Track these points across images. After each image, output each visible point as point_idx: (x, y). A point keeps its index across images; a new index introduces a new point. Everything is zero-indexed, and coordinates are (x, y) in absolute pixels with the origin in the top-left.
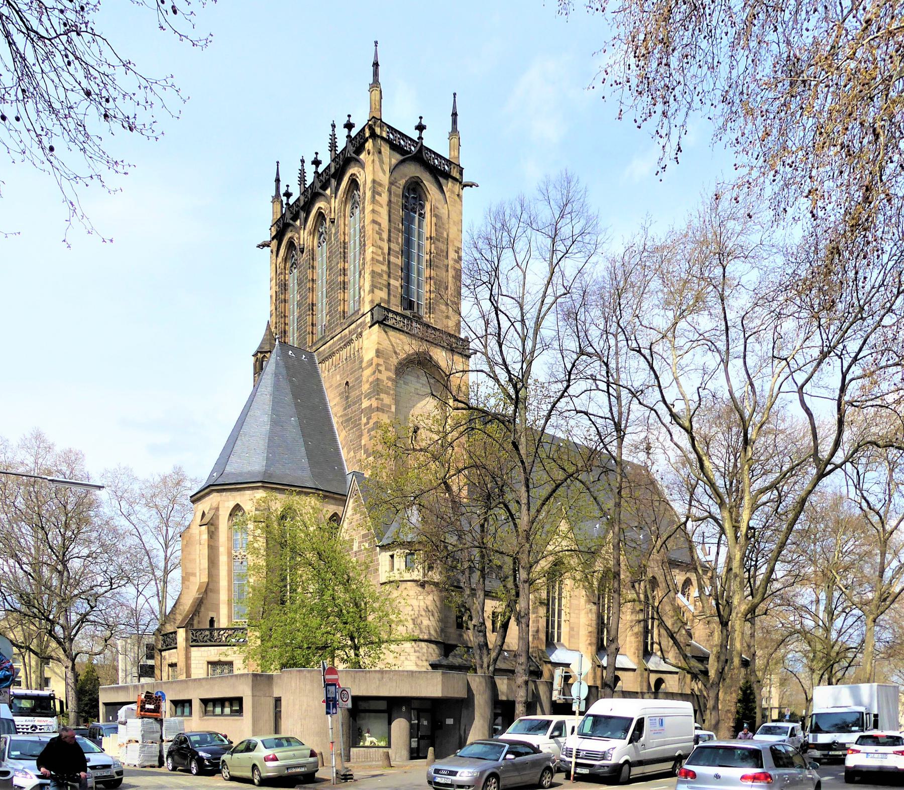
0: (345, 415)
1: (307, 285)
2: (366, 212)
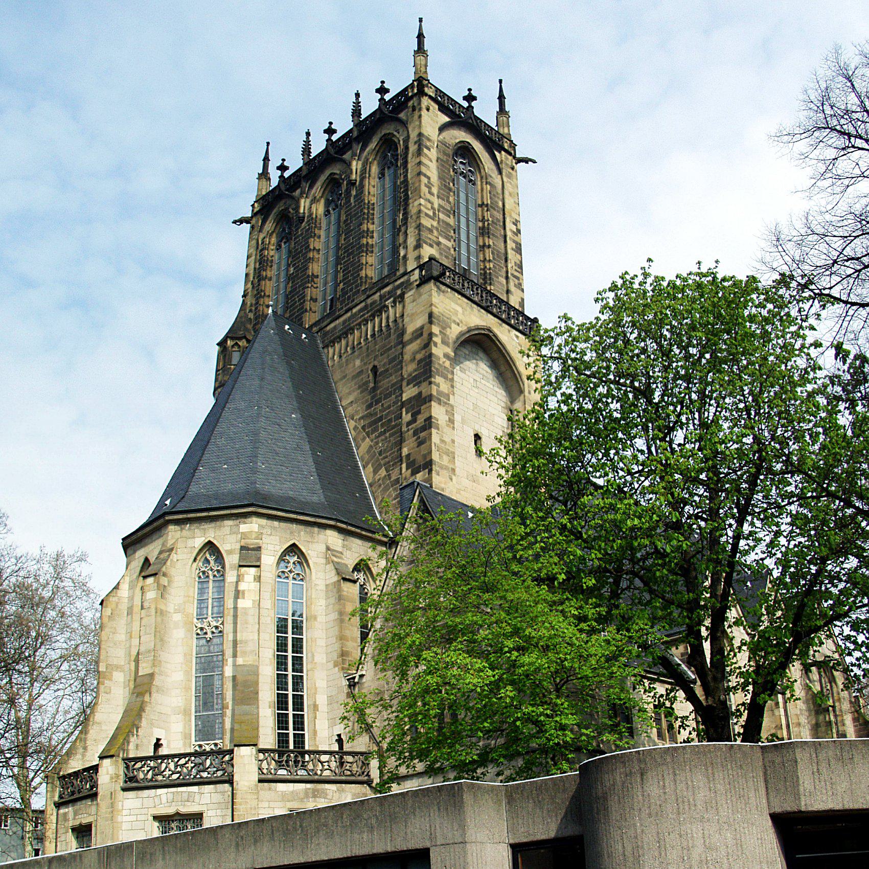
0: (371, 415)
1: (299, 257)
2: (409, 166)
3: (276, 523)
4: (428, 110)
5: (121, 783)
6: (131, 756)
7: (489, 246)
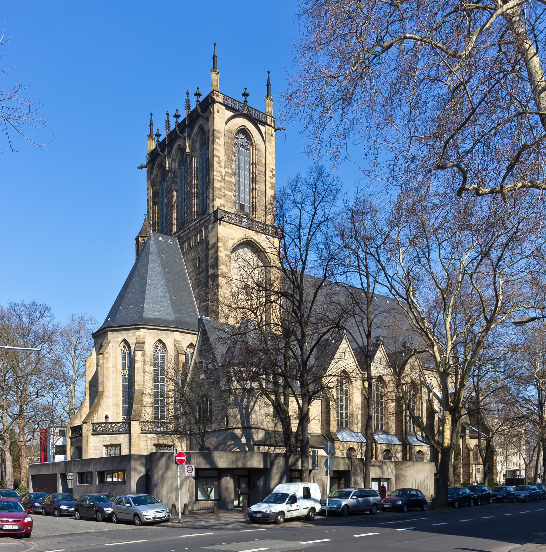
3: (151, 331)
4: (218, 112)
5: (91, 432)
6: (95, 422)
7: (256, 189)
